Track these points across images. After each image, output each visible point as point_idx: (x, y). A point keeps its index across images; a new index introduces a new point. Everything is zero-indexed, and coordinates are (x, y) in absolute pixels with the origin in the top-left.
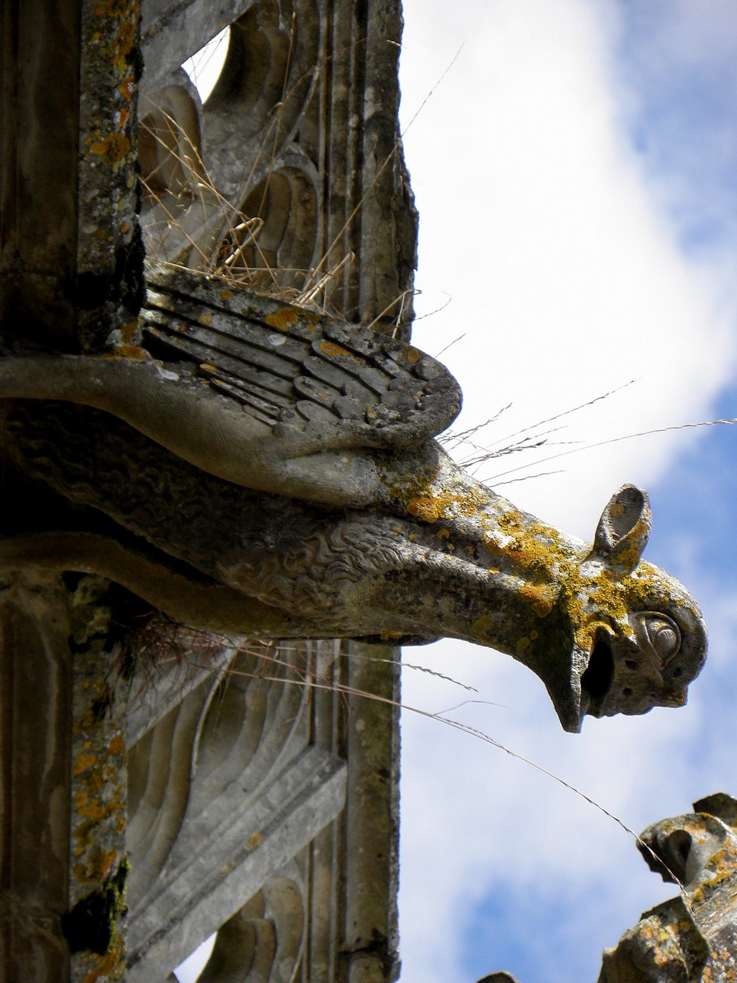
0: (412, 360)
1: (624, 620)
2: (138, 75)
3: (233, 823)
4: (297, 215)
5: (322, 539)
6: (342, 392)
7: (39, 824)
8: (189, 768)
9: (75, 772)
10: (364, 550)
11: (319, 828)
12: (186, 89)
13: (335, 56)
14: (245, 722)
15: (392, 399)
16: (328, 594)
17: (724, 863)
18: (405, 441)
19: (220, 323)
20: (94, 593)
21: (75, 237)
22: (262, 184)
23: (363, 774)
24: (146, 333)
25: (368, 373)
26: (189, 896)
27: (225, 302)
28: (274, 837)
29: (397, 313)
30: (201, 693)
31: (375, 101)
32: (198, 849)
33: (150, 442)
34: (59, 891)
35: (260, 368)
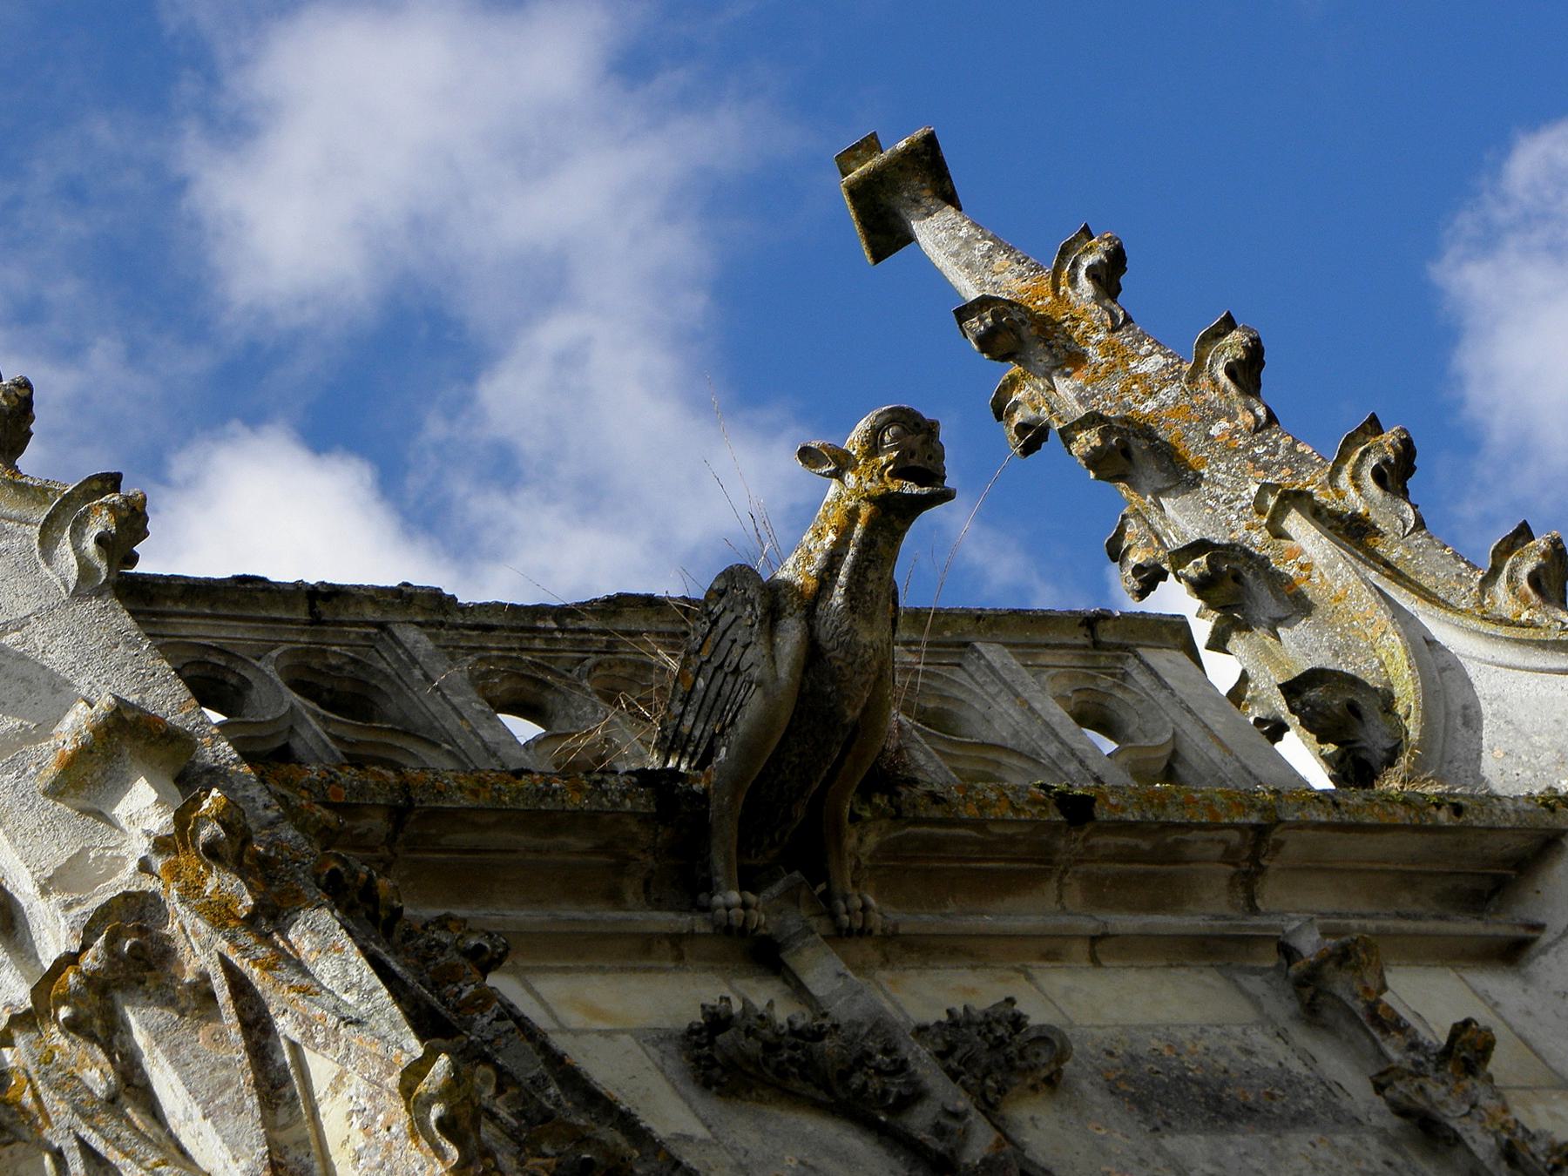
0: (714, 596)
1: (884, 459)
2: (528, 772)
3: (1010, 715)
4: (619, 671)
5: (829, 655)
6: (734, 641)
7: (1011, 840)
8: (975, 743)
9: (978, 816)
10: (837, 627)
11: (1014, 661)
12: (537, 742)
13: (516, 646)
14: (946, 707)
15: (739, 609)
16: (866, 651)
17: (1036, 402)
18: (766, 600)
19: (689, 721)
20: (863, 803)
21: (633, 814)
22: (598, 692)
23: (979, 632)
24: (695, 768)
25: (722, 624)
26: (1057, 744)
27: (675, 717)
28: (1020, 689)
29: (683, 607)
30: (926, 735)
31: (545, 620)
32: (1027, 739)
33: (766, 766)
34: (1056, 827)
35: (719, 694)
